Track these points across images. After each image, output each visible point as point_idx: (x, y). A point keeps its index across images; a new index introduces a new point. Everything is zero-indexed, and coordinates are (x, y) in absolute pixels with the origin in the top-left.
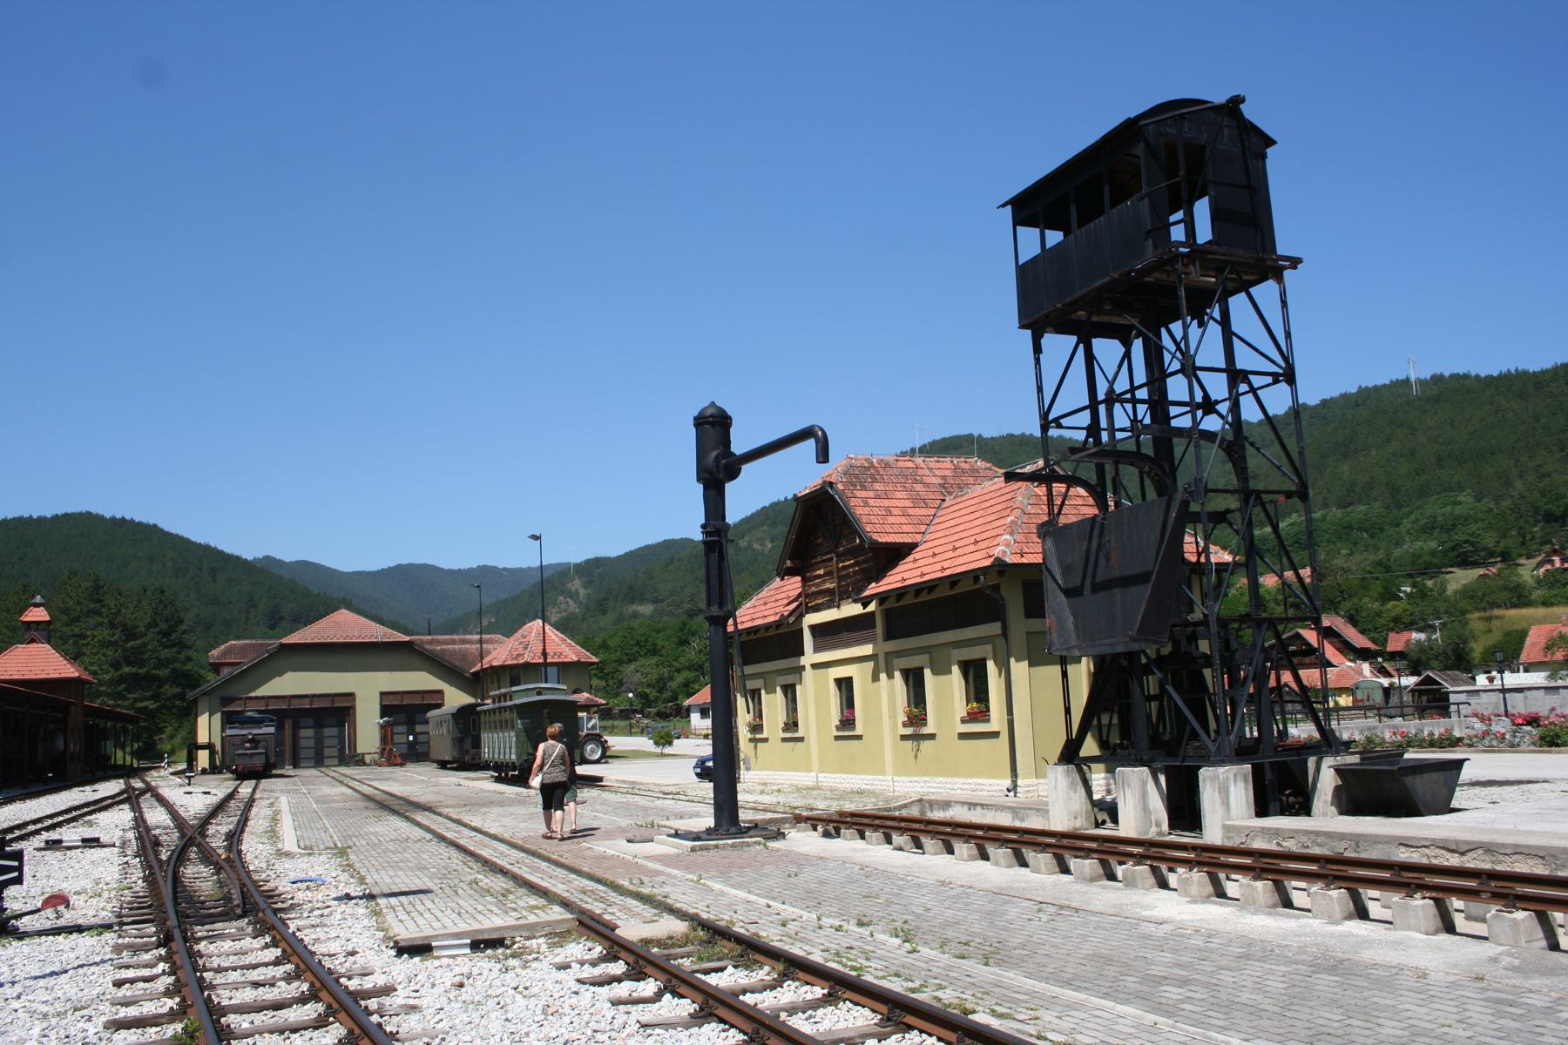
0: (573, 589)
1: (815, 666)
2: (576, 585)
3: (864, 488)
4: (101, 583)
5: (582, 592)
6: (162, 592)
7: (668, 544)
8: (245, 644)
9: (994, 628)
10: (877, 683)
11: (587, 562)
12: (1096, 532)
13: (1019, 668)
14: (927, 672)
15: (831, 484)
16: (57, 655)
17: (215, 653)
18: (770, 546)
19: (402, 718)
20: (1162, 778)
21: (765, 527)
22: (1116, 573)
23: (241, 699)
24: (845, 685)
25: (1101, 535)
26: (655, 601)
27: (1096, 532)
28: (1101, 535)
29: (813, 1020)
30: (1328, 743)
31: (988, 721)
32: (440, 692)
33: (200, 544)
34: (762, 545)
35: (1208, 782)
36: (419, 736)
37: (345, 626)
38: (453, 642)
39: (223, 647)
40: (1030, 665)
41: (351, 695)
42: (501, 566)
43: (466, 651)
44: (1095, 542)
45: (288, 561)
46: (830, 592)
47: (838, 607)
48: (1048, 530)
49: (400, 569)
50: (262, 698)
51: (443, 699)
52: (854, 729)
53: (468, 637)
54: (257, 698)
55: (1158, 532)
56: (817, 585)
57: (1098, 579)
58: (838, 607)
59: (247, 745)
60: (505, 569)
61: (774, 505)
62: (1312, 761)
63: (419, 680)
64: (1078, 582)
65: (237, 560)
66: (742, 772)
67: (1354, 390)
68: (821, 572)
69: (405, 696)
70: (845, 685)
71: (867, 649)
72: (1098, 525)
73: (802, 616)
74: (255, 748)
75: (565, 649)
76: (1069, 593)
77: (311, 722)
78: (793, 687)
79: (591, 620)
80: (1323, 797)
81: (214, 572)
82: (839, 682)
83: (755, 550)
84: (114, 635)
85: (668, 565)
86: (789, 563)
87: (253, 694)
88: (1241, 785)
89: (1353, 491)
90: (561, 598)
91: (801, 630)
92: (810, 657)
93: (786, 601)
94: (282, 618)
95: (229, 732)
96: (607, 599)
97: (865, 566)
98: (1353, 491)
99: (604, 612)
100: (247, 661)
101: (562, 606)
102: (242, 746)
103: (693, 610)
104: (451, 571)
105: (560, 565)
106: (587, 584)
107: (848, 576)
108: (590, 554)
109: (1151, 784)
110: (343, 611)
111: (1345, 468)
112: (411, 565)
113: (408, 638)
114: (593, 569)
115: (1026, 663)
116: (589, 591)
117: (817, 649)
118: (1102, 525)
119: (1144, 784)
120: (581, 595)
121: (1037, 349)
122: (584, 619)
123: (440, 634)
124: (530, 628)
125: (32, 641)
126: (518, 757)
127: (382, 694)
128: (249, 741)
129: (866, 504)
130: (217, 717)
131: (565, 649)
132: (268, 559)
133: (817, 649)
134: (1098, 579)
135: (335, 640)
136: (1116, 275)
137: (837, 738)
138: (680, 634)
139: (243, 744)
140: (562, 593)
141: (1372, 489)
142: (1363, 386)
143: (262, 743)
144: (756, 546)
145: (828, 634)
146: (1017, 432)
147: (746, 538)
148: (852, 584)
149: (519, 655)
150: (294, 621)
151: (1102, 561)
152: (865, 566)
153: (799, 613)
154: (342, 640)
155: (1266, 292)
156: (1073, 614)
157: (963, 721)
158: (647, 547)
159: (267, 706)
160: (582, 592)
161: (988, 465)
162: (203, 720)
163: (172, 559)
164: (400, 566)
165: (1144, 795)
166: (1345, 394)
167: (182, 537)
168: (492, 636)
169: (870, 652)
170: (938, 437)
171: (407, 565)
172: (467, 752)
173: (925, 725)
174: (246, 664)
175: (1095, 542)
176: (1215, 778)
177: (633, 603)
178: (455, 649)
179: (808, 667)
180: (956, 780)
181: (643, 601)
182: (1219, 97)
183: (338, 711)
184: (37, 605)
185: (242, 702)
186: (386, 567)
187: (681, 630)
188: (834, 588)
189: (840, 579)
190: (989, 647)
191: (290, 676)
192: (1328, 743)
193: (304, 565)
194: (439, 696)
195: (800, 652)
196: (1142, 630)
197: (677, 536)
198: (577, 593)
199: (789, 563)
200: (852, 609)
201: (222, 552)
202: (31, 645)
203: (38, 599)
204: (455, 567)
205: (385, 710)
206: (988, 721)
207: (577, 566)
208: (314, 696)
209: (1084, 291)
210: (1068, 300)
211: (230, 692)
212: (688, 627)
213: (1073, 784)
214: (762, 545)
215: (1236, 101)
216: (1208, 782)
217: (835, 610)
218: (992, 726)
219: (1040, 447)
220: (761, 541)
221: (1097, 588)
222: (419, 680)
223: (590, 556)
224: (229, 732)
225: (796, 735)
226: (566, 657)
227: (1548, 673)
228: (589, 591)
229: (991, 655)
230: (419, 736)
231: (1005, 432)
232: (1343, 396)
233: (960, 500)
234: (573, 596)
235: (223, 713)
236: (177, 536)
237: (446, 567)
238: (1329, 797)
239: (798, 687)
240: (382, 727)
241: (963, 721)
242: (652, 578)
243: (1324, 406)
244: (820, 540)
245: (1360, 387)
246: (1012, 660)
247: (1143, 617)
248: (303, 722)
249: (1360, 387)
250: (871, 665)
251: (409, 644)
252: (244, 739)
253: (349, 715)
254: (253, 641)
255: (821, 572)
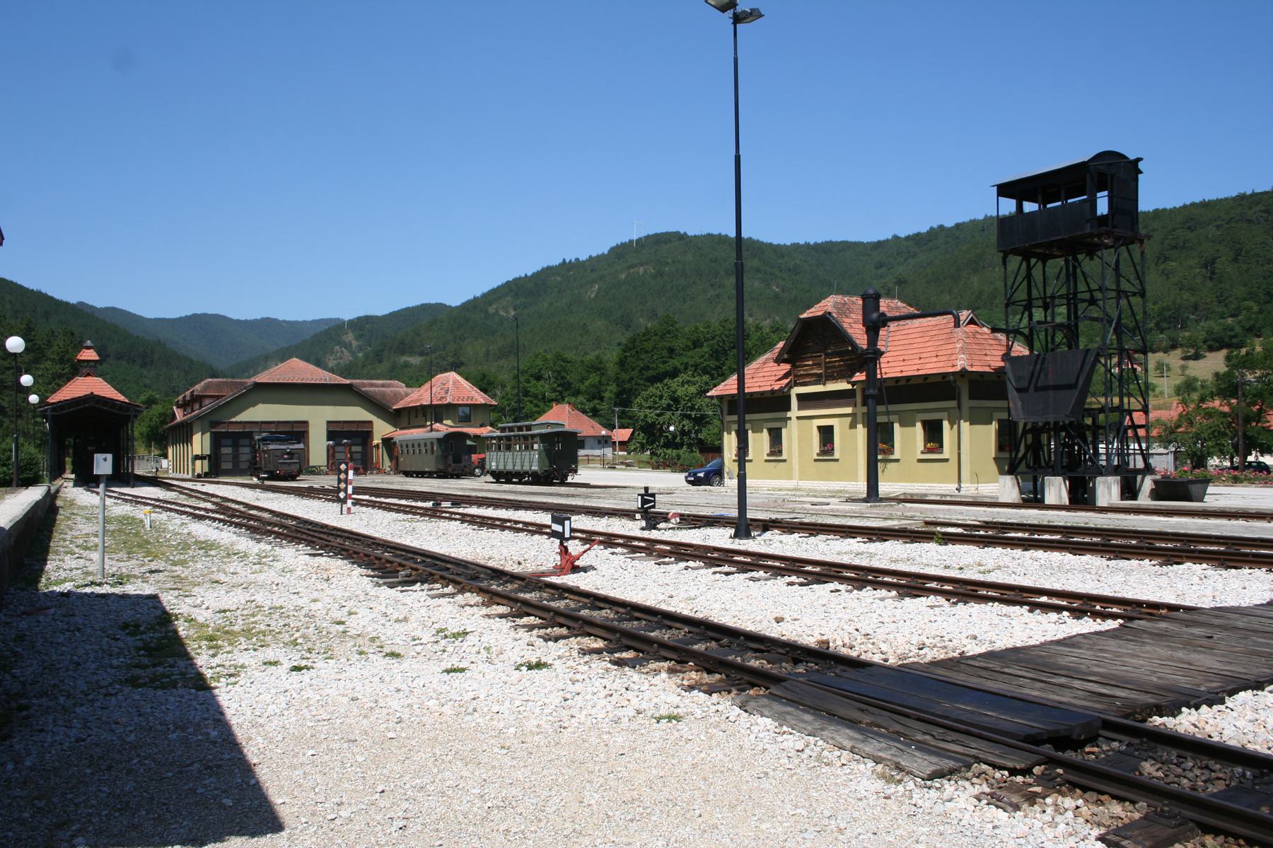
0: (347, 340)
1: (798, 418)
2: (350, 337)
3: (847, 317)
4: (32, 326)
5: (355, 343)
6: (72, 334)
7: (425, 308)
8: (219, 382)
9: (953, 404)
10: (853, 430)
11: (359, 319)
12: (1039, 362)
13: (965, 426)
14: (896, 426)
15: (829, 313)
16: (109, 386)
17: (198, 387)
18: (513, 313)
19: (359, 440)
20: (1067, 482)
21: (509, 298)
22: (1051, 383)
23: (225, 423)
24: (826, 434)
25: (1043, 363)
26: (421, 354)
27: (1039, 362)
28: (1043, 363)
29: (982, 568)
30: (1148, 469)
31: (942, 453)
32: (371, 422)
33: (32, 290)
34: (507, 312)
35: (1101, 484)
36: (354, 455)
37: (298, 370)
38: (372, 385)
39: (203, 383)
40: (971, 424)
41: (306, 423)
42: (281, 319)
43: (384, 392)
44: (1038, 367)
45: (99, 307)
46: (819, 375)
47: (824, 384)
48: (1006, 357)
49: (195, 317)
50: (241, 422)
51: (372, 428)
52: (833, 455)
53: (374, 381)
54: (236, 422)
55: (1079, 365)
56: (806, 370)
57: (1039, 385)
58: (824, 384)
59: (286, 456)
60: (284, 321)
61: (516, 280)
62: (1139, 478)
63: (356, 413)
64: (1026, 385)
65: (67, 304)
66: (726, 480)
67: (981, 217)
68: (811, 363)
69: (345, 425)
70: (826, 434)
71: (849, 410)
72: (1041, 358)
73: (791, 387)
74: (291, 459)
75: (471, 394)
76: (1019, 390)
77: (229, 442)
78: (779, 430)
79: (369, 367)
80: (1144, 494)
81: (47, 315)
82: (820, 428)
83: (501, 316)
84: (63, 369)
85: (431, 325)
86: (786, 356)
87: (233, 420)
88: (1116, 486)
89: (980, 298)
90: (338, 347)
91: (789, 397)
92: (794, 412)
93: (777, 378)
94: (108, 356)
95: (301, 446)
96: (383, 350)
97: (849, 362)
98: (980, 298)
99: (380, 361)
100: (230, 395)
101: (338, 355)
102: (282, 457)
103: (455, 363)
104: (238, 321)
105: (331, 320)
106: (358, 338)
107: (834, 367)
108: (362, 313)
109: (1063, 485)
110: (295, 359)
111: (975, 280)
112: (205, 315)
113: (348, 382)
114: (363, 325)
115: (968, 423)
116: (360, 343)
117: (800, 408)
118: (1044, 359)
119: (1060, 484)
120: (354, 346)
121: (1004, 263)
122: (364, 366)
123: (378, 379)
124: (447, 377)
125: (88, 375)
126: (540, 468)
127: (329, 422)
128: (288, 454)
129: (852, 327)
130: (207, 436)
131: (471, 394)
132: (81, 303)
133: (800, 408)
134: (1039, 385)
135: (294, 381)
136: (1066, 237)
137: (816, 460)
138: (481, 383)
139: (283, 456)
140: (339, 343)
141: (996, 298)
142: (989, 215)
143: (296, 456)
144: (502, 313)
145: (805, 400)
146: (716, 232)
147: (494, 306)
148: (837, 372)
149: (442, 398)
150: (118, 359)
151: (1042, 376)
152: (849, 362)
153: (790, 386)
154: (299, 381)
155: (1135, 248)
156: (1021, 401)
157: (922, 453)
158: (408, 309)
159: (245, 428)
160: (355, 343)
161: (905, 305)
162: (197, 438)
163: (10, 302)
164: (195, 315)
165: (1060, 490)
166: (974, 220)
167: (16, 284)
168: (392, 382)
169: (850, 412)
170: (651, 233)
171: (201, 314)
172: (450, 465)
173: (893, 454)
174: (229, 397)
175: (1038, 367)
176: (1105, 482)
177: (403, 354)
178: (375, 391)
179: (794, 418)
180: (914, 484)
181: (412, 352)
182: (1132, 157)
183: (298, 432)
184: (88, 348)
185: (226, 425)
186: (183, 315)
187: (482, 380)
188: (821, 373)
189: (827, 368)
190: (946, 414)
191: (260, 407)
192: (1148, 469)
193: (113, 310)
194: (368, 425)
195: (789, 409)
196: (1072, 412)
197: (433, 301)
198: (351, 344)
199: (786, 356)
200: (843, 386)
201: (52, 298)
202: (88, 378)
203: (89, 343)
204: (242, 318)
205: (331, 435)
206: (942, 453)
207: (351, 322)
208: (279, 422)
209: (1044, 240)
210: (1033, 243)
211: (216, 418)
212: (487, 378)
213: (1014, 485)
214: (507, 312)
215: (1139, 159)
216: (1101, 484)
217: (822, 386)
218: (945, 455)
219: (734, 246)
220: (505, 309)
221: (1037, 389)
222: (356, 413)
223: (362, 313)
224: (301, 446)
225: (780, 458)
226: (476, 400)
227: (725, 433)
228: (360, 343)
229: (946, 417)
230: (354, 455)
231: (705, 232)
232: (973, 222)
233: (902, 328)
234: (347, 346)
235: (212, 433)
236: (12, 282)
237: (235, 317)
238: (1148, 494)
239: (784, 431)
240: (328, 447)
241: (922, 453)
242: (419, 335)
243: (958, 228)
244: (810, 344)
245: (986, 216)
246: (962, 422)
247: (1073, 406)
248: (224, 442)
249: (986, 216)
250: (850, 419)
251: (349, 386)
252: (284, 452)
253: (303, 437)
254: (225, 380)
255: (811, 363)
